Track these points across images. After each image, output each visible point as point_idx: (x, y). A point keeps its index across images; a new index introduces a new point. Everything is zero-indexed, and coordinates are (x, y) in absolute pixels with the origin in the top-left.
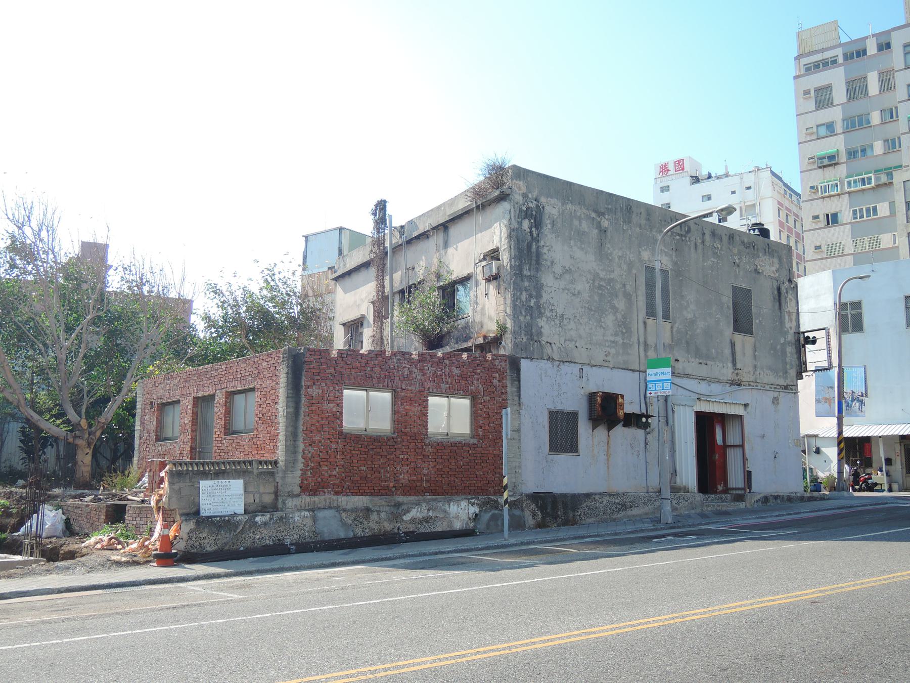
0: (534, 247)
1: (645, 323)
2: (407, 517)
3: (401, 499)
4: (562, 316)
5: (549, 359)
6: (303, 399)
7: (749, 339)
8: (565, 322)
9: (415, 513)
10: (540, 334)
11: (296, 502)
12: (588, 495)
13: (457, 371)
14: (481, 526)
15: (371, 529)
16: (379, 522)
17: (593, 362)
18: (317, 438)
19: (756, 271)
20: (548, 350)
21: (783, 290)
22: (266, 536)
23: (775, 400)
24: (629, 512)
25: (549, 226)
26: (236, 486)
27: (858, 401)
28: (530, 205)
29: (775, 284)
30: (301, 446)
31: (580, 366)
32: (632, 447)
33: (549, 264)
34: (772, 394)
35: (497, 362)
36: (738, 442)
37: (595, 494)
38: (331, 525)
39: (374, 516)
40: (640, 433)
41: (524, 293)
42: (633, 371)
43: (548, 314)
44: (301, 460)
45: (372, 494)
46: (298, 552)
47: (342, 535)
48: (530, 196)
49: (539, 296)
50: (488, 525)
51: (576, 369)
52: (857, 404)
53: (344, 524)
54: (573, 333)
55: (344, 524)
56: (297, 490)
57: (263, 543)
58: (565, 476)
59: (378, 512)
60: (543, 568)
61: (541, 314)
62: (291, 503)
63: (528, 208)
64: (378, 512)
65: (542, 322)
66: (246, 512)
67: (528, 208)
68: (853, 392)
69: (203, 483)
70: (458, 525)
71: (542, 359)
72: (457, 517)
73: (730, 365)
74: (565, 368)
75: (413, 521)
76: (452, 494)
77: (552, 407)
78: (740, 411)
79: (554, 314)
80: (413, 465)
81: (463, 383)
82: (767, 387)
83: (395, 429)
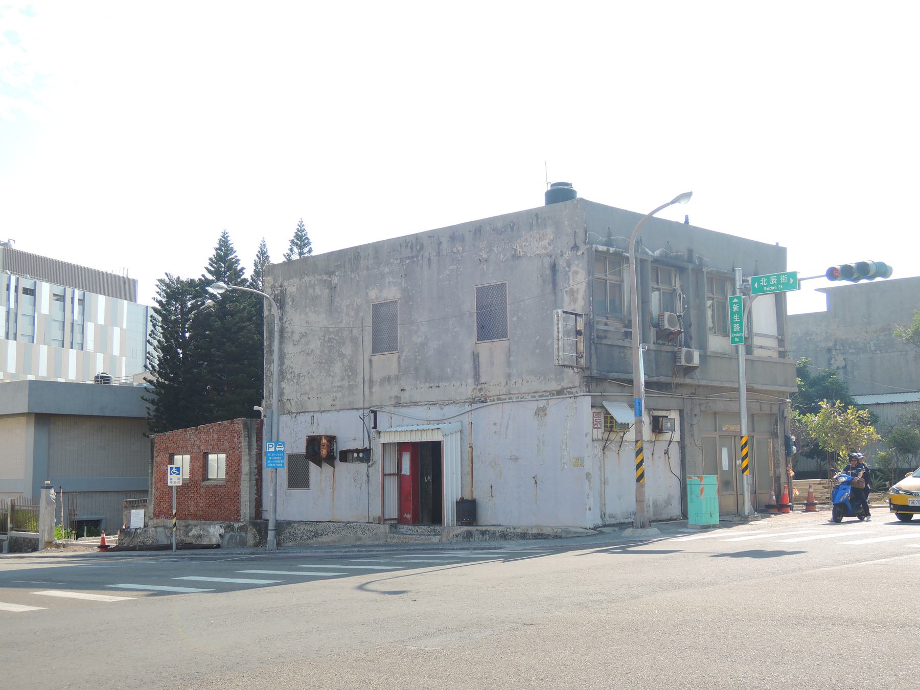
1: (371, 361)
2: (190, 534)
3: (191, 522)
4: (299, 375)
7: (499, 346)
17: (322, 409)
19: (516, 257)
21: (562, 263)
23: (541, 412)
29: (547, 261)
31: (312, 414)
34: (534, 405)
36: (387, 479)
43: (288, 376)
70: (214, 541)
73: (470, 381)
75: (194, 536)
82: (529, 397)
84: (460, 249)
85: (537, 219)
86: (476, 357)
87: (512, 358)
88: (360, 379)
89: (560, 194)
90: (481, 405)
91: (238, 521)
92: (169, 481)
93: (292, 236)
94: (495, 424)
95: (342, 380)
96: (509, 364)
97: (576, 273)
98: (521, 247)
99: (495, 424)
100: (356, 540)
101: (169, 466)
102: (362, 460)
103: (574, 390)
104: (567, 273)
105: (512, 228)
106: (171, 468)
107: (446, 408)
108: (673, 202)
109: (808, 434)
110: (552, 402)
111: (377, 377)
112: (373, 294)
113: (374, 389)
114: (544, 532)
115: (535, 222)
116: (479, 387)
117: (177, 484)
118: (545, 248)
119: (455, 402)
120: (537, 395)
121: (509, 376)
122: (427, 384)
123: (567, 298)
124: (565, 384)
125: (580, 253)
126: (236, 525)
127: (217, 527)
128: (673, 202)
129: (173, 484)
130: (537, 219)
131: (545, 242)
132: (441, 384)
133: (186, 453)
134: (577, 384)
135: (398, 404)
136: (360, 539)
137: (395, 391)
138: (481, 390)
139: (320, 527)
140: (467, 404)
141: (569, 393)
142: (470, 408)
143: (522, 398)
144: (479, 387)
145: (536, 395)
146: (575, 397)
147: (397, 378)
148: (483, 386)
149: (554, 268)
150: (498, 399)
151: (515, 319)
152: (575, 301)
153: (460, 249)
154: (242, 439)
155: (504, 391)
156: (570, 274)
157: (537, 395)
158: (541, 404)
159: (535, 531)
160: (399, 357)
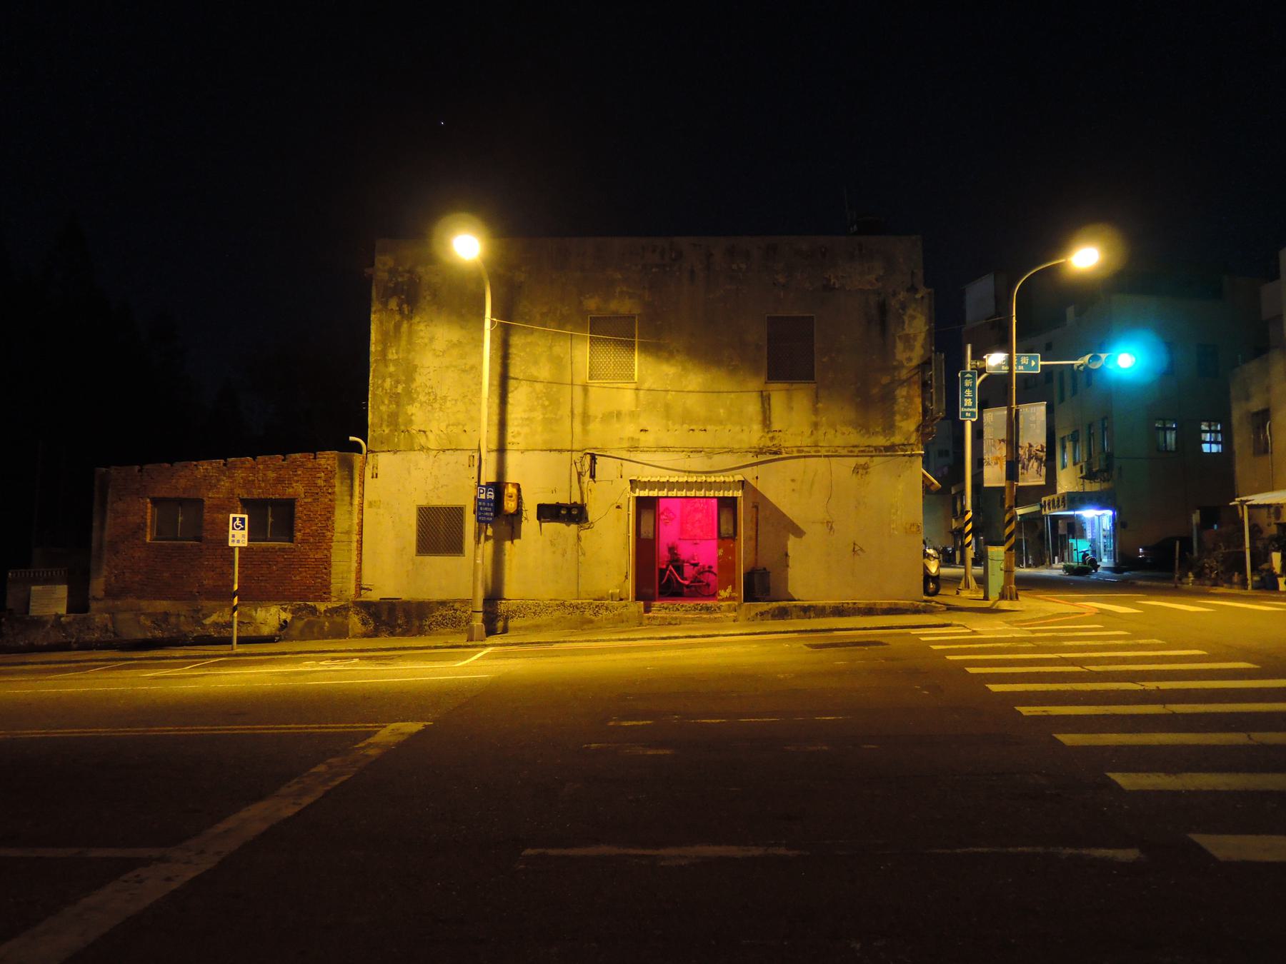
2: (207, 621)
5: (422, 448)
10: (410, 422)
11: (101, 605)
12: (443, 603)
20: (422, 440)
32: (552, 544)
33: (426, 340)
34: (852, 462)
37: (455, 601)
41: (388, 380)
42: (560, 451)
43: (422, 398)
49: (410, 379)
50: (302, 632)
52: (1036, 465)
54: (461, 417)
59: (178, 615)
61: (412, 400)
63: (397, 284)
65: (411, 409)
67: (397, 284)
70: (266, 631)
71: (412, 449)
72: (264, 623)
73: (756, 427)
75: (216, 624)
79: (432, 397)
84: (744, 266)
88: (566, 411)
92: (231, 539)
95: (532, 409)
97: (913, 318)
107: (716, 458)
109: (486, 500)
111: (595, 410)
116: (771, 435)
117: (240, 545)
122: (686, 427)
125: (918, 296)
126: (322, 607)
129: (235, 544)
132: (708, 428)
142: (755, 460)
145: (856, 450)
147: (633, 415)
148: (776, 434)
153: (744, 266)
154: (337, 482)
155: (808, 441)
156: (906, 318)
157: (853, 450)
158: (862, 461)
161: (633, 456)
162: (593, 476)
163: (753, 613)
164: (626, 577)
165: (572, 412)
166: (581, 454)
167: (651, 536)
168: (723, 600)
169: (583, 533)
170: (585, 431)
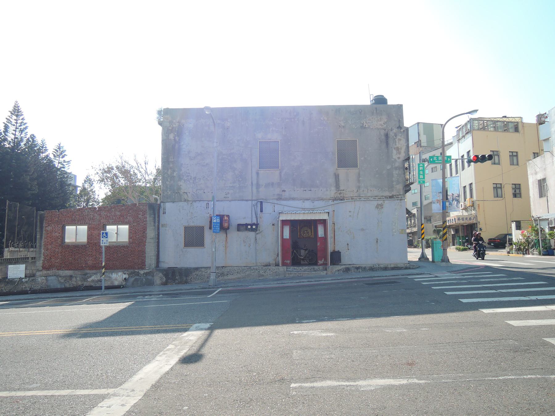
0: (177, 146)
1: (258, 174)
2: (89, 280)
3: (88, 271)
4: (195, 178)
5: (185, 201)
6: (44, 232)
7: (353, 172)
8: (197, 181)
9: (93, 278)
11: (40, 273)
12: (197, 269)
13: (118, 213)
14: (129, 283)
15: (73, 285)
16: (77, 281)
18: (50, 247)
19: (363, 127)
21: (391, 134)
22: (27, 287)
24: (226, 277)
25: (187, 134)
26: (22, 267)
27: (456, 200)
28: (174, 126)
29: (383, 132)
30: (43, 251)
34: (375, 203)
35: (141, 207)
37: (202, 268)
38: (54, 282)
39: (74, 279)
40: (252, 234)
41: (170, 170)
44: (42, 256)
45: (74, 270)
46: (31, 293)
47: (59, 286)
48: (174, 121)
50: (133, 284)
51: (204, 204)
52: (455, 203)
53: (60, 282)
55: (60, 282)
56: (41, 268)
57: (26, 289)
58: (193, 258)
59: (76, 277)
60: (14, 309)
62: (38, 274)
63: (173, 128)
64: (76, 277)
66: (26, 276)
67: (173, 128)
68: (453, 195)
69: (10, 266)
70: (116, 283)
72: (116, 280)
73: (333, 188)
74: (196, 204)
75: (93, 281)
76: (114, 269)
77: (186, 225)
78: (325, 217)
79: (189, 178)
80: (94, 257)
81: (121, 218)
82: (372, 199)
83: (88, 242)
85: (376, 110)
86: (337, 177)
87: (361, 178)
89: (380, 100)
90: (340, 201)
91: (143, 269)
92: (101, 242)
93: (11, 109)
94: (350, 212)
96: (359, 181)
97: (400, 140)
98: (366, 123)
99: (350, 212)
100: (259, 277)
101: (102, 232)
102: (252, 230)
103: (400, 196)
104: (394, 139)
105: (360, 113)
106: (103, 233)
108: (466, 113)
110: (386, 202)
112: (259, 135)
113: (260, 190)
114: (399, 266)
115: (375, 111)
116: (339, 192)
118: (382, 126)
119: (322, 199)
120: (375, 197)
121: (359, 187)
122: (302, 189)
123: (395, 152)
124: (394, 193)
125: (402, 130)
126: (142, 272)
127: (120, 274)
128: (466, 113)
130: (376, 110)
131: (382, 123)
132: (312, 189)
133: (124, 223)
134: (401, 193)
135: (280, 198)
136: (263, 276)
137: (277, 191)
138: (340, 194)
139: (225, 271)
140: (331, 201)
141: (397, 198)
143: (367, 199)
144: (339, 192)
146: (401, 200)
148: (342, 192)
149: (387, 136)
150: (352, 199)
151: (362, 159)
152: (400, 153)
155: (356, 195)
156: (397, 140)
157: (375, 197)
159: (392, 266)
160: (280, 173)
161: (278, 202)
162: (261, 211)
163: (334, 270)
164: (278, 255)
165: (252, 183)
166: (256, 202)
167: (323, 236)
168: (320, 265)
169: (258, 236)
170: (258, 191)
